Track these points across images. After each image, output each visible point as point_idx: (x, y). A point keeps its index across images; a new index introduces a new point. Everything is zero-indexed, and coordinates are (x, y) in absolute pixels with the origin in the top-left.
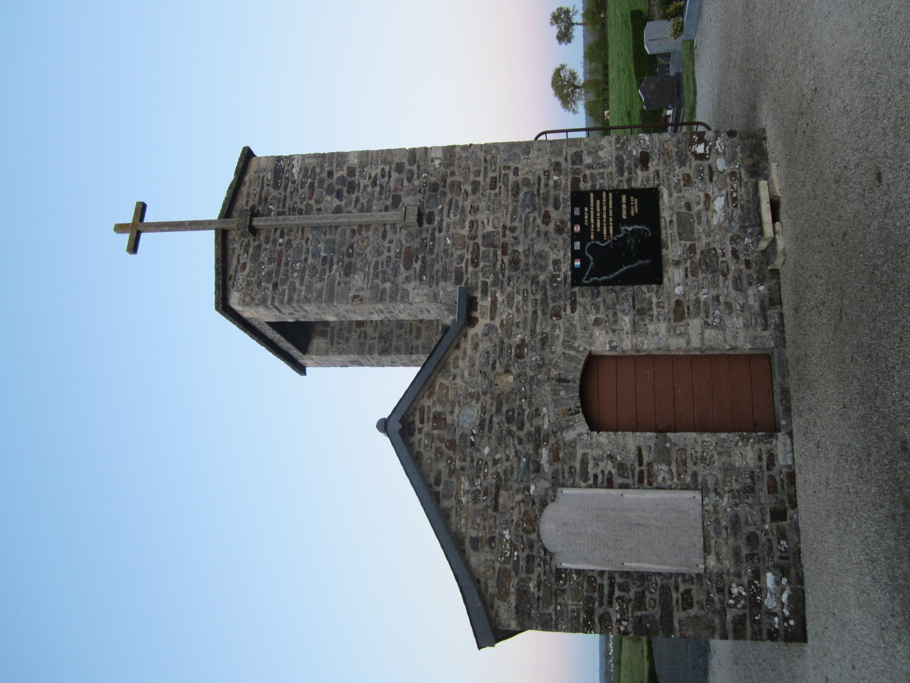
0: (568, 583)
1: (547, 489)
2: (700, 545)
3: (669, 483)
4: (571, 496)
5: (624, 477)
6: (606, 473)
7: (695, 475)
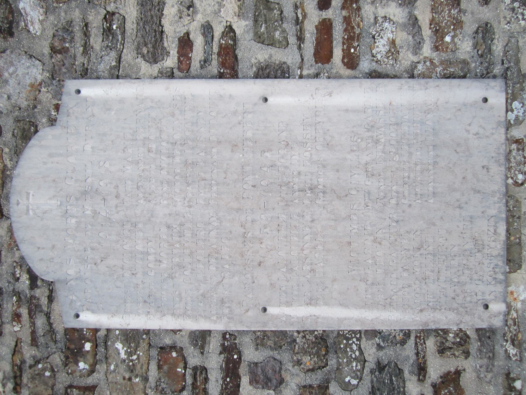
0: (101, 368)
1: (36, 87)
2: (497, 246)
3: (407, 58)
4: (106, 105)
5: (272, 43)
6: (218, 30)
7: (485, 32)
